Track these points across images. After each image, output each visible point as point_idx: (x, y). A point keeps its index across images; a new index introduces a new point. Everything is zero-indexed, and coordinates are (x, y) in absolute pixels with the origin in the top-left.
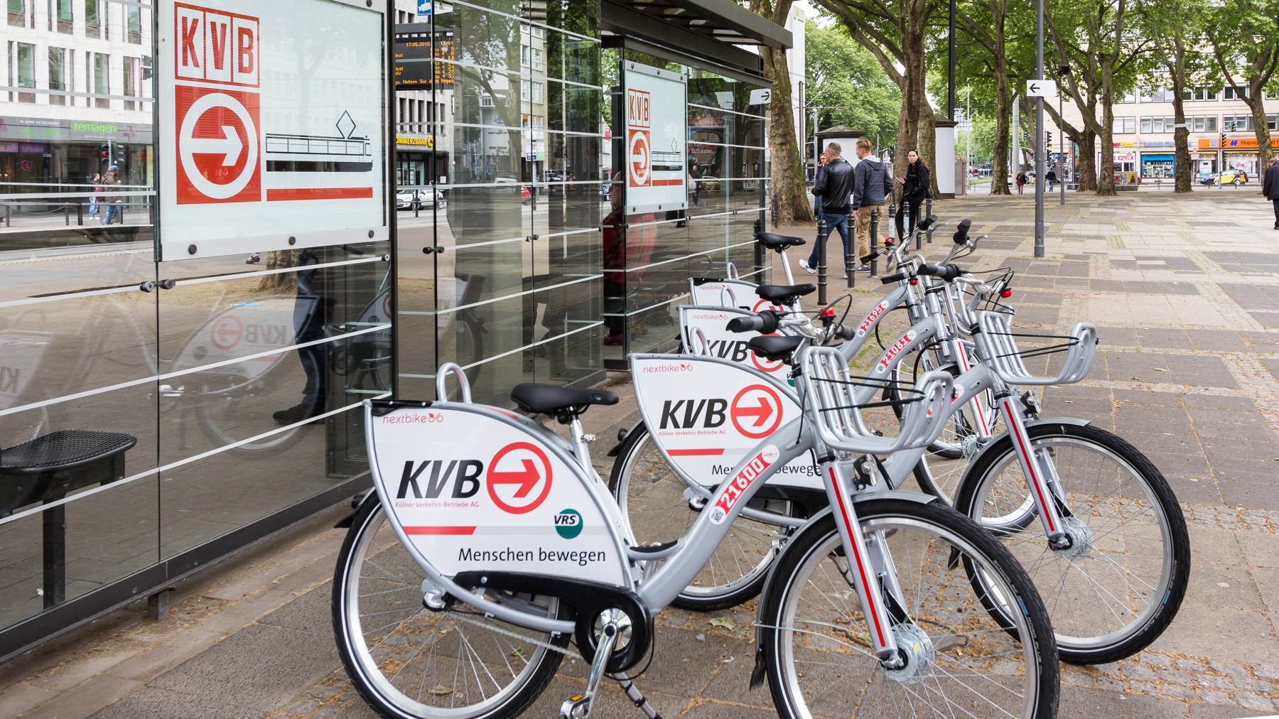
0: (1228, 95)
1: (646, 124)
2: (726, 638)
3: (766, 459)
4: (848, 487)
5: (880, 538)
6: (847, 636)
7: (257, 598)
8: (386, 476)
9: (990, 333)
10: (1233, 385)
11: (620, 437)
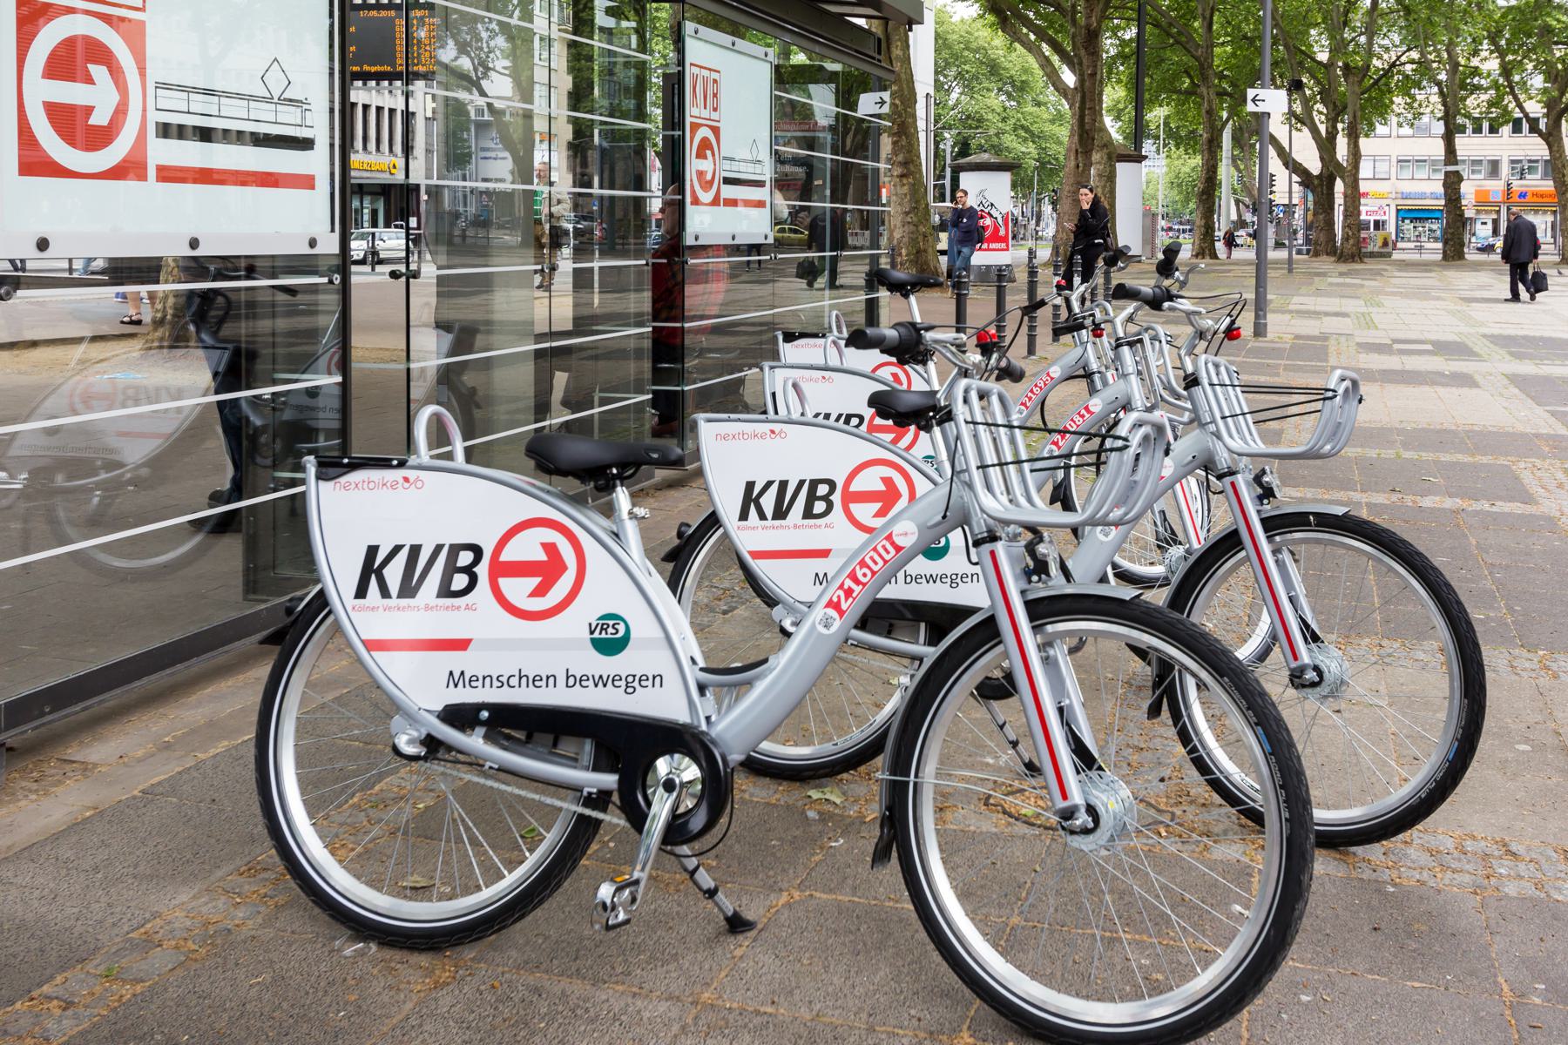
0: (1517, 128)
1: (715, 116)
2: (831, 816)
3: (899, 541)
4: (1016, 578)
5: (1060, 652)
6: (1005, 812)
7: (140, 760)
8: (338, 565)
9: (1212, 385)
10: (1528, 499)
11: (680, 535)
